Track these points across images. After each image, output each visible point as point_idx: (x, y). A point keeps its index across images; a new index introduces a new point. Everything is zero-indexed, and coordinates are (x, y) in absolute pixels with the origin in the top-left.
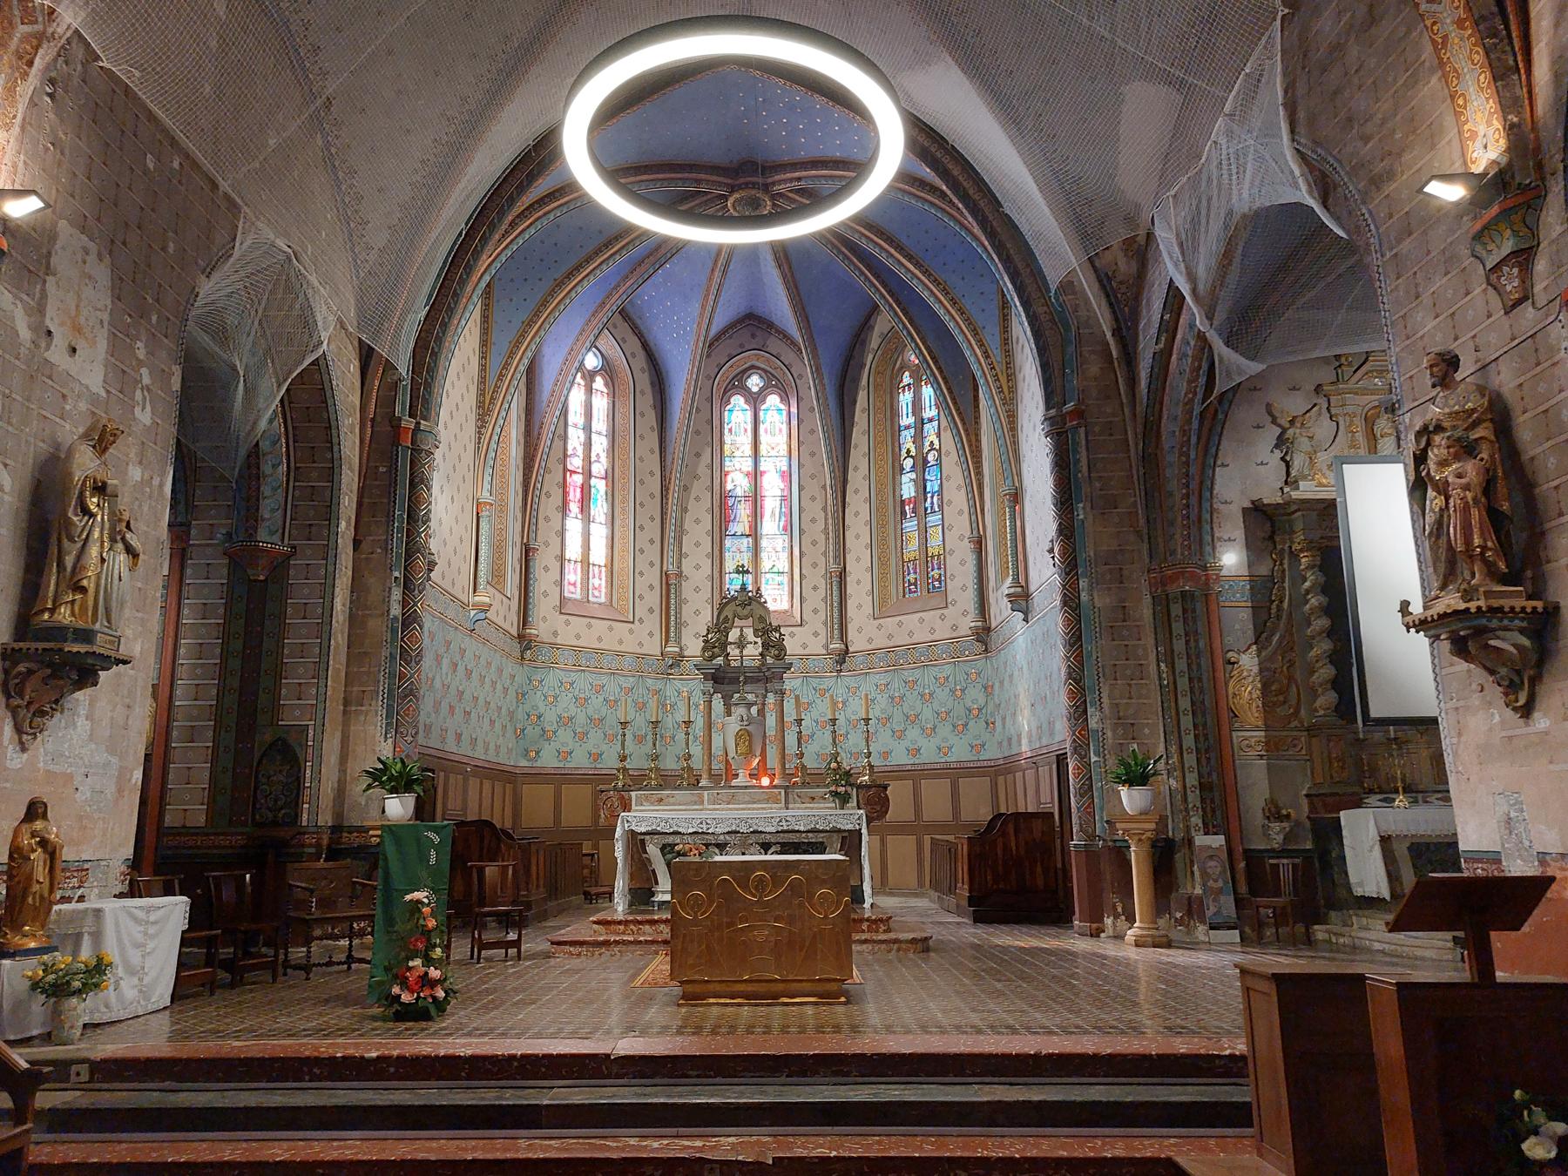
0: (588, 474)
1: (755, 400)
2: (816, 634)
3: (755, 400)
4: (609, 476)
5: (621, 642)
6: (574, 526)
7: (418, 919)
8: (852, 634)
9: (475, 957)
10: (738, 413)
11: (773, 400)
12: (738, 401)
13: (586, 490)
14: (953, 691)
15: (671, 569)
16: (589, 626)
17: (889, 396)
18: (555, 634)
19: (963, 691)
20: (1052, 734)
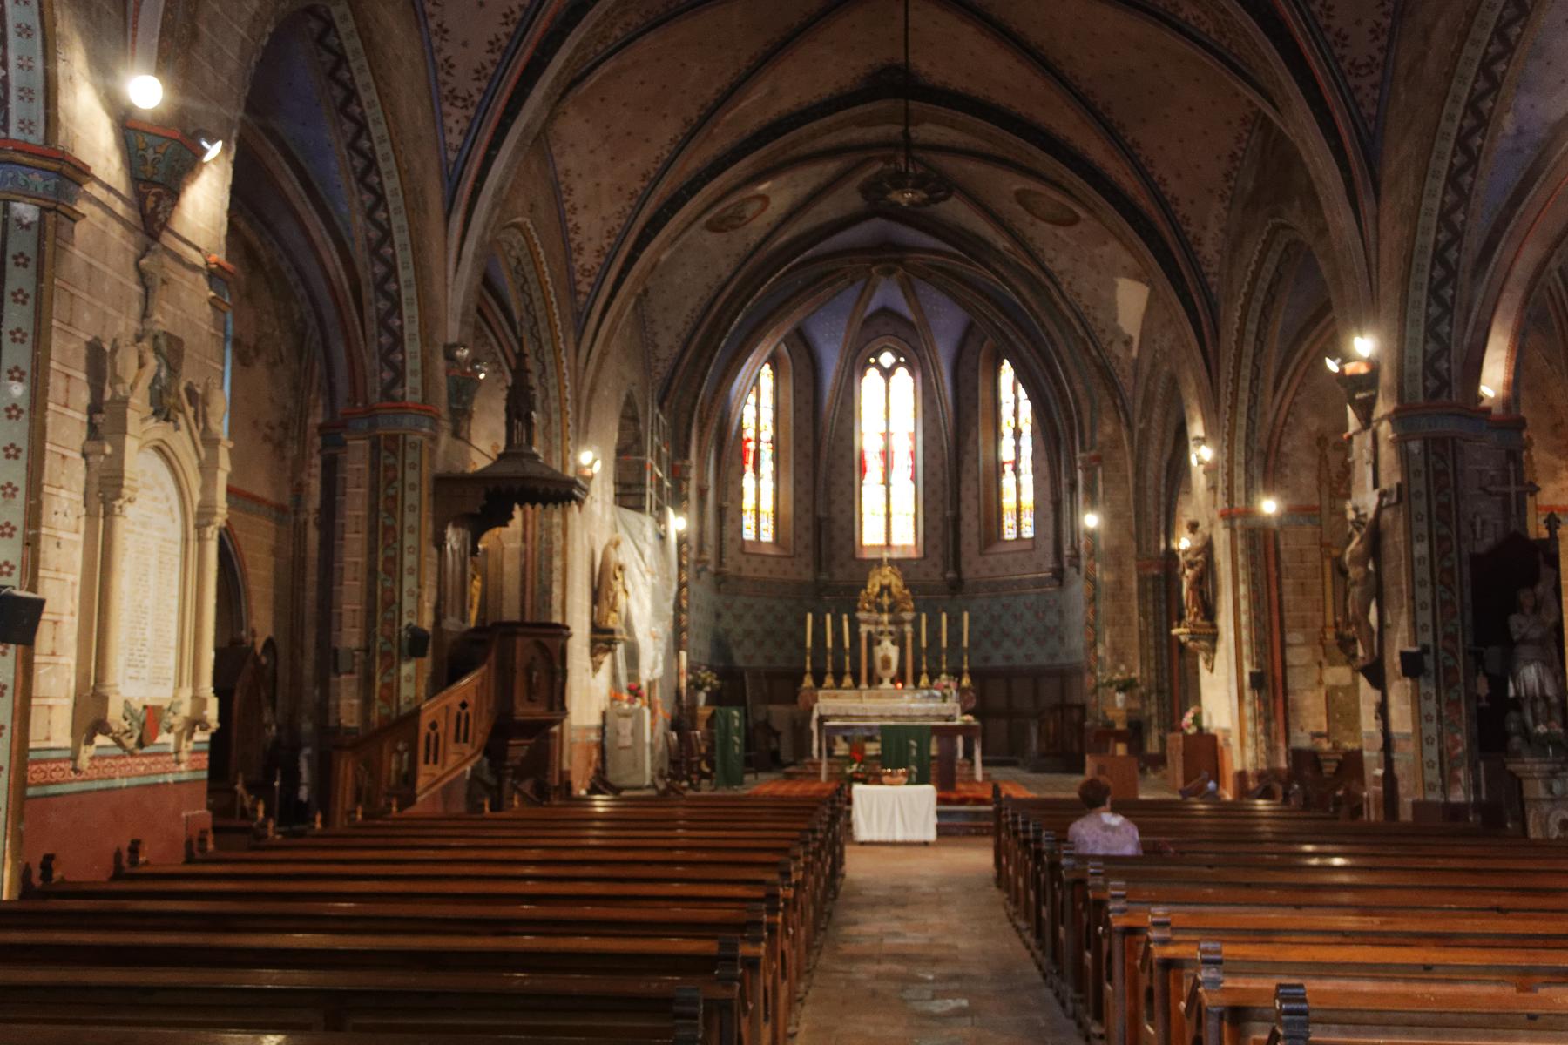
0: (758, 441)
1: (887, 373)
2: (935, 565)
3: (887, 373)
4: (775, 442)
5: (771, 572)
6: (748, 481)
7: (1148, 950)
8: (964, 566)
9: (775, 858)
10: (871, 383)
11: (902, 374)
12: (872, 373)
13: (757, 453)
14: (1037, 614)
15: (822, 514)
16: (763, 562)
17: (1406, 391)
18: (740, 569)
19: (1044, 612)
20: (51, 443)
